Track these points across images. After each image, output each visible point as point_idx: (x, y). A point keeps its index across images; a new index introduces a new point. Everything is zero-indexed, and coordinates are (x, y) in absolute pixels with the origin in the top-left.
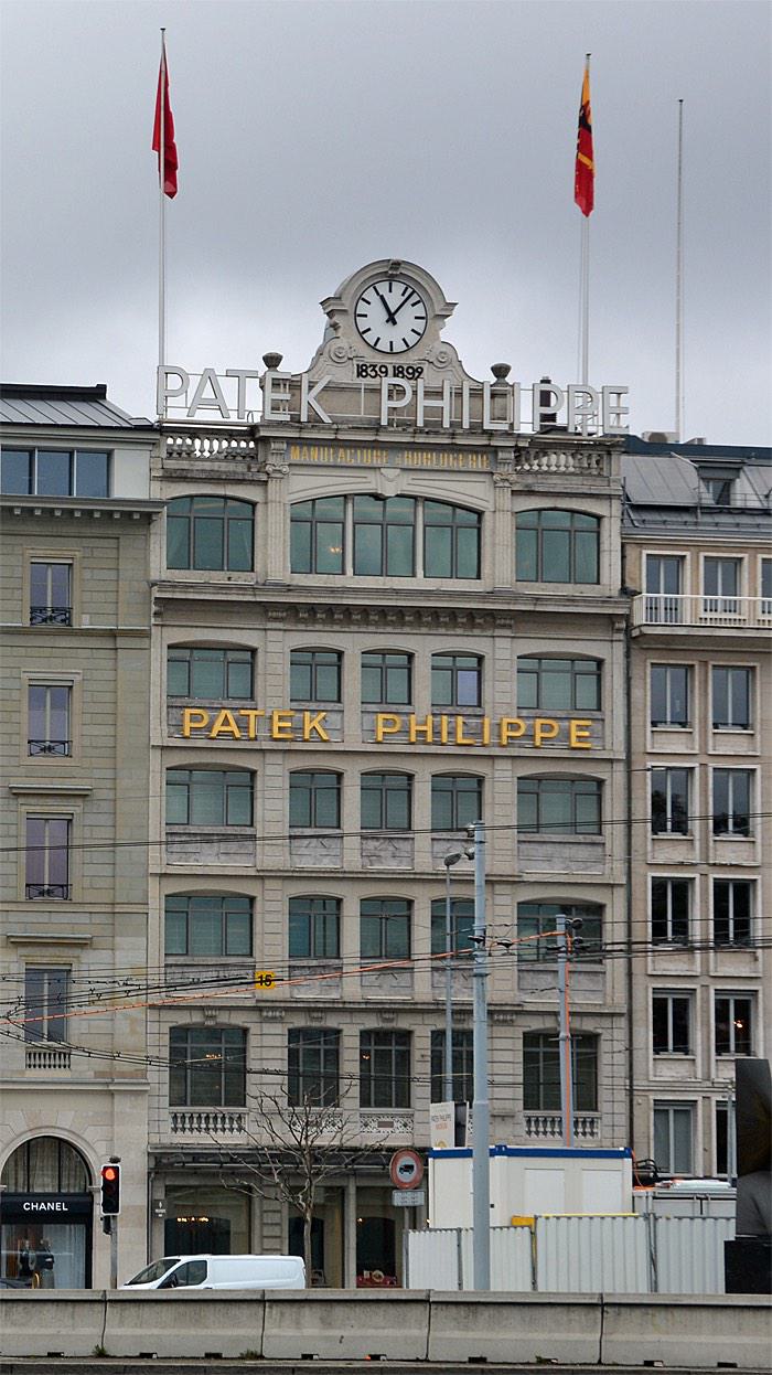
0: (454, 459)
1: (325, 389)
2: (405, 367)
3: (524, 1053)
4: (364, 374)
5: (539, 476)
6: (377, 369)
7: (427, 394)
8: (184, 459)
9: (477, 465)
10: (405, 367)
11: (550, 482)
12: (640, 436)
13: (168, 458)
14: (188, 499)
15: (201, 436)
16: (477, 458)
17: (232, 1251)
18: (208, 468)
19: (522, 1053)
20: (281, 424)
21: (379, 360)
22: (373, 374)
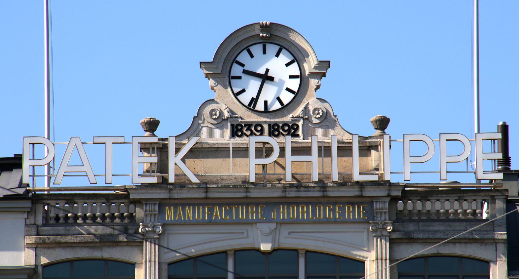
0: (330, 210)
1: (191, 151)
2: (281, 125)
3: (325, 157)
4: (240, 133)
5: (421, 224)
6: (253, 129)
7: (296, 151)
8: (61, 225)
9: (354, 215)
10: (281, 125)
11: (432, 228)
12: (237, 137)
13: (44, 225)
14: (69, 263)
15: (77, 201)
16: (354, 209)
17: (319, 158)
18: (214, 185)
19: (325, 158)
20: (151, 186)
21: (253, 118)
22: (249, 133)
